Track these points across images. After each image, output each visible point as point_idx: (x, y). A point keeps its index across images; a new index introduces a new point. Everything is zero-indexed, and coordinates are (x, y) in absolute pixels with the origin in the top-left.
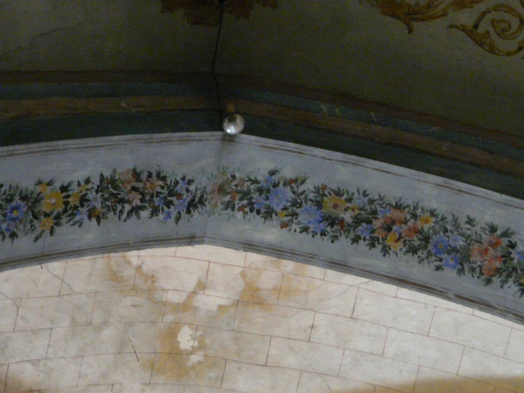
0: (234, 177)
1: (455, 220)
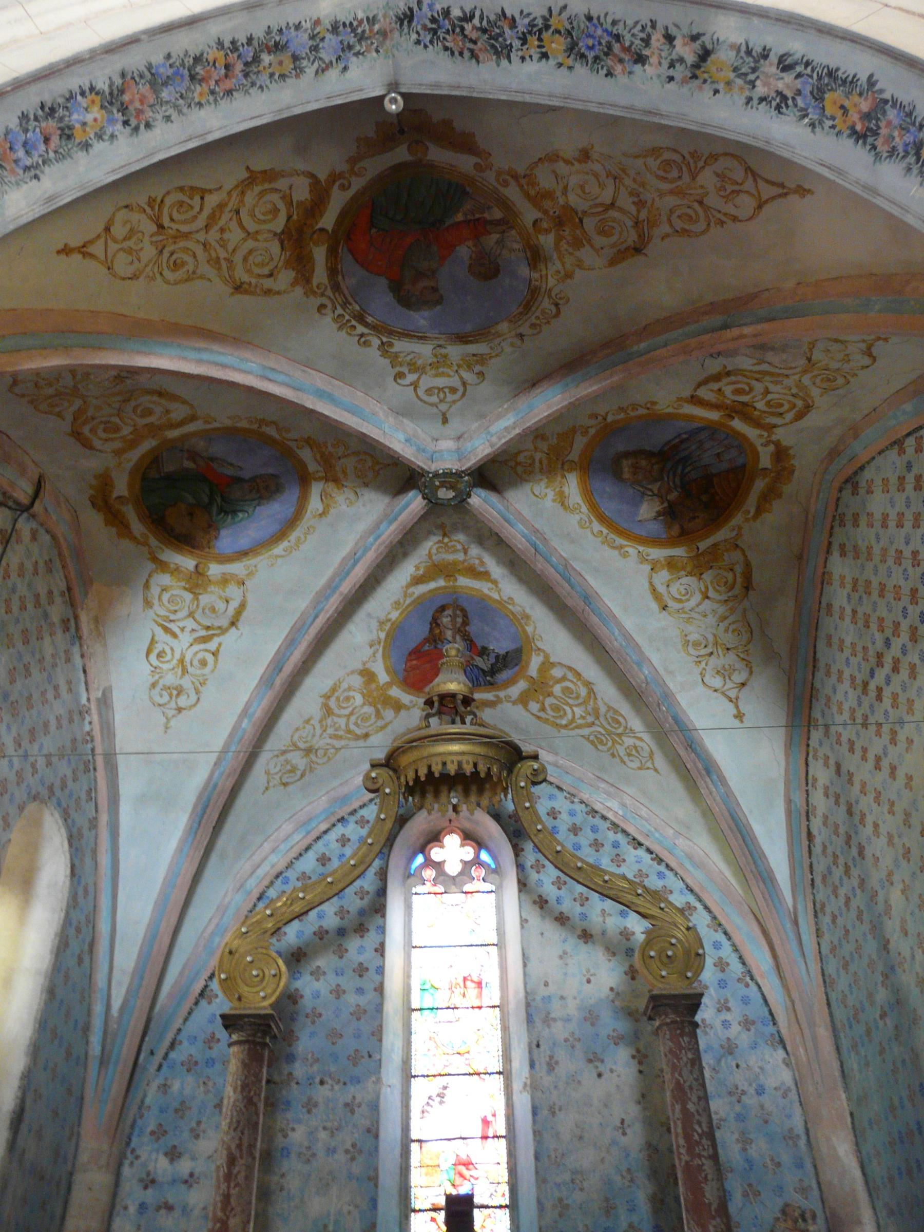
0: (377, 51)
1: (180, 112)
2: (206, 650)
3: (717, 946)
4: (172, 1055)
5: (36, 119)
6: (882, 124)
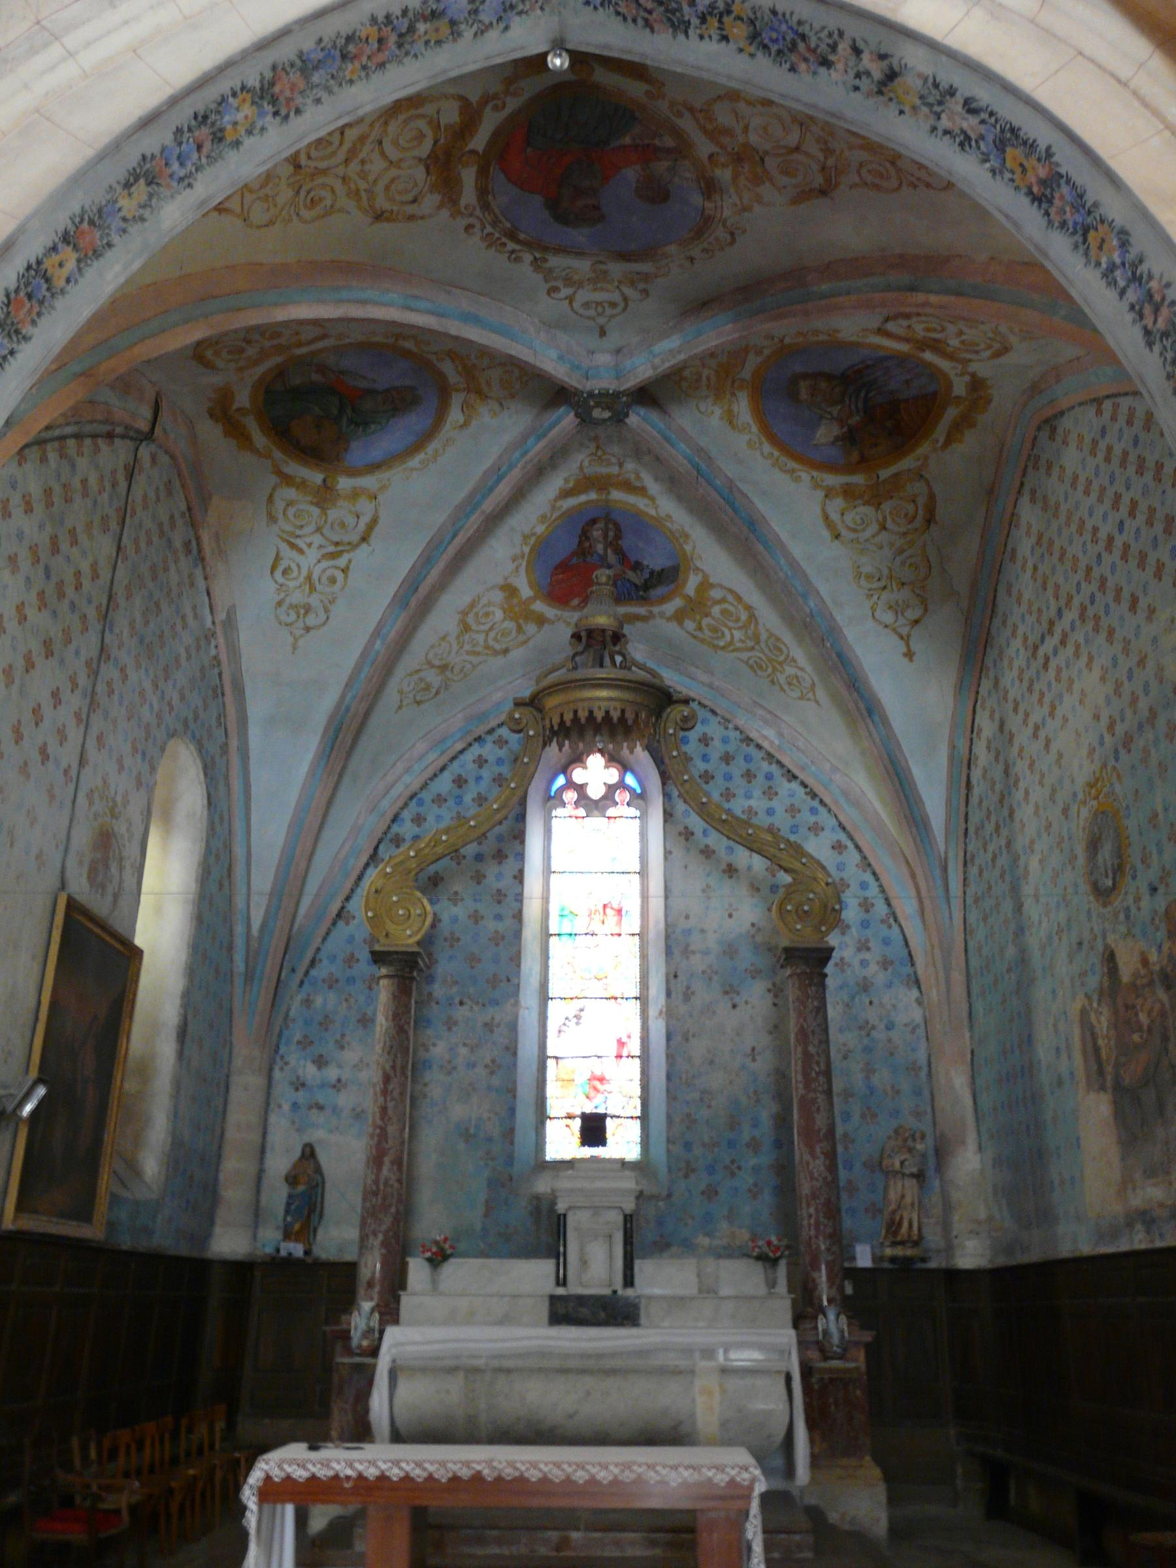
0: (542, 9)
1: (330, 92)
2: (336, 567)
3: (864, 886)
4: (313, 973)
5: (190, 130)
6: (1057, 195)
